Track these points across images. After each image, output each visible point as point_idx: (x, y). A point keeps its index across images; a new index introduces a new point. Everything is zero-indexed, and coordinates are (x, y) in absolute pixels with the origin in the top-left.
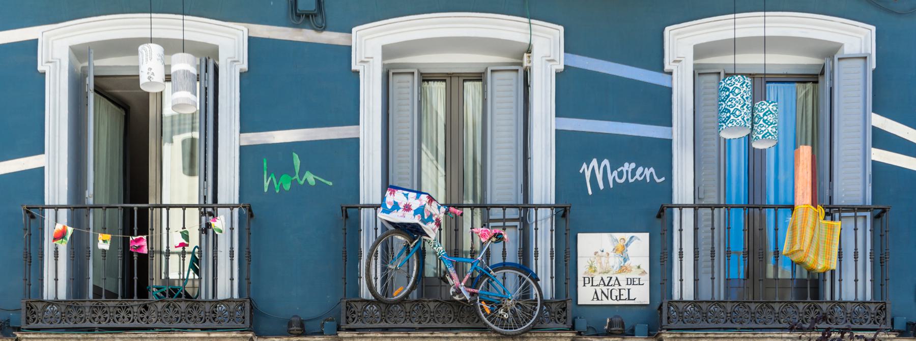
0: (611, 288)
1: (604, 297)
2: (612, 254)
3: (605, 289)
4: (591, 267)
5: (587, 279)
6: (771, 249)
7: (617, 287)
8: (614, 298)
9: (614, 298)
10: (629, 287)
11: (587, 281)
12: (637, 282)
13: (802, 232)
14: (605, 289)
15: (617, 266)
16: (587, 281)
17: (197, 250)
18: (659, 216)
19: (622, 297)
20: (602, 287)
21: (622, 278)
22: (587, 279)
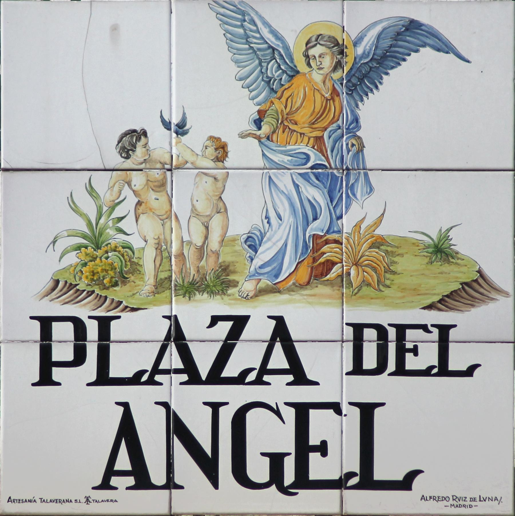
0: (235, 396)
1: (185, 464)
2: (245, 152)
3: (192, 404)
4: (151, 209)
5: (63, 332)
6: (173, 15)
7: (279, 390)
8: (258, 469)
9: (258, 469)
10: (367, 388)
11: (63, 352)
12: (428, 356)
13: (413, 37)
14: (192, 404)
15: (281, 238)
16: (63, 352)
17: (229, 36)
18: (158, 199)
19: (319, 468)
20: (174, 390)
21: (318, 321)
22: (63, 332)
